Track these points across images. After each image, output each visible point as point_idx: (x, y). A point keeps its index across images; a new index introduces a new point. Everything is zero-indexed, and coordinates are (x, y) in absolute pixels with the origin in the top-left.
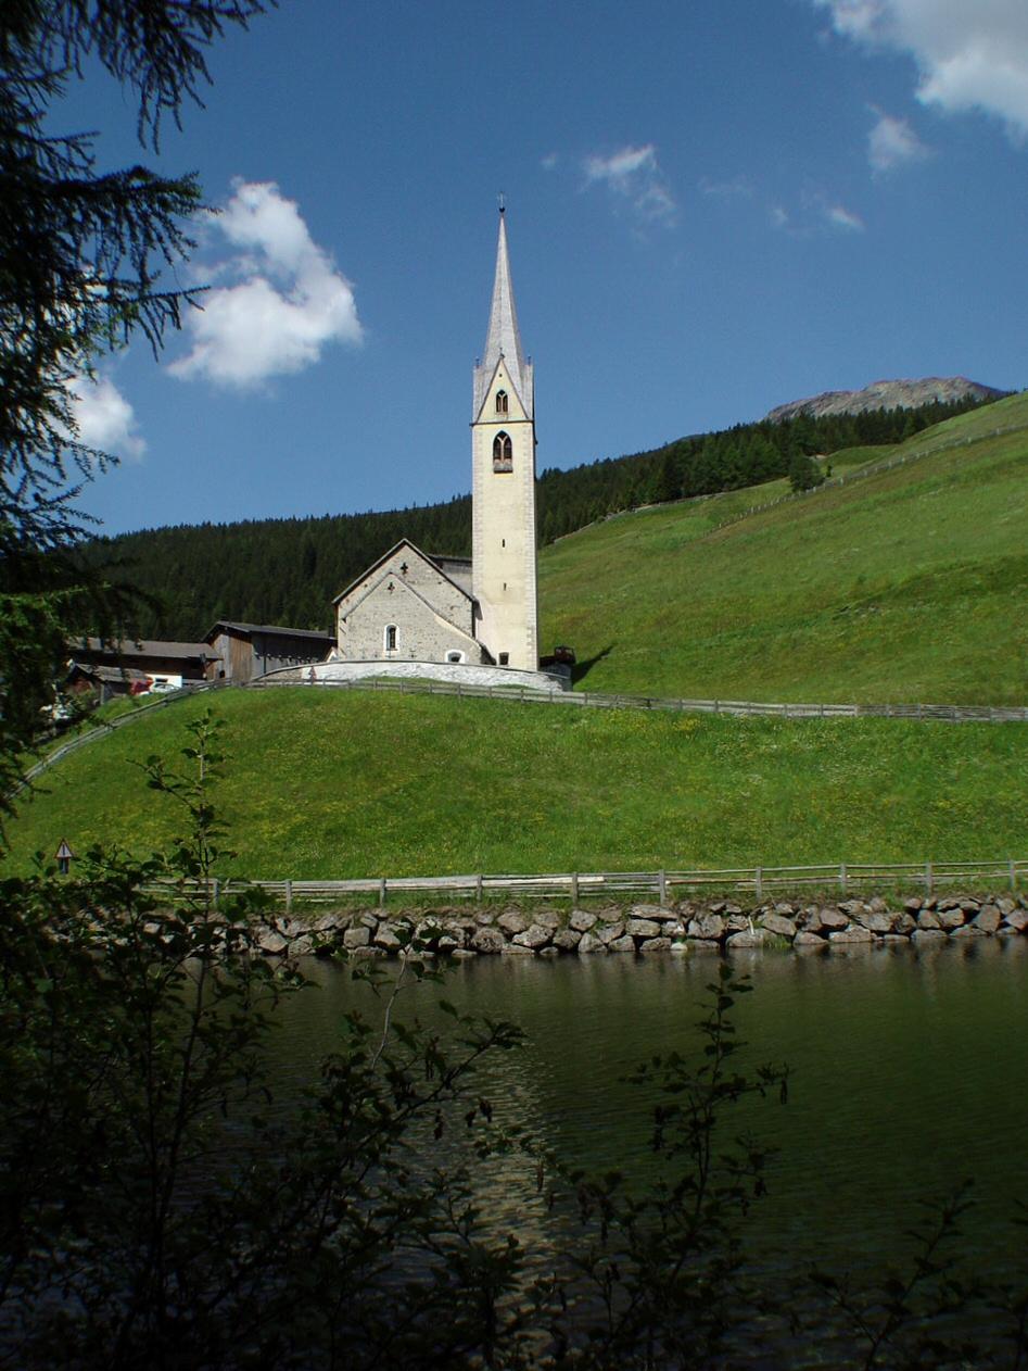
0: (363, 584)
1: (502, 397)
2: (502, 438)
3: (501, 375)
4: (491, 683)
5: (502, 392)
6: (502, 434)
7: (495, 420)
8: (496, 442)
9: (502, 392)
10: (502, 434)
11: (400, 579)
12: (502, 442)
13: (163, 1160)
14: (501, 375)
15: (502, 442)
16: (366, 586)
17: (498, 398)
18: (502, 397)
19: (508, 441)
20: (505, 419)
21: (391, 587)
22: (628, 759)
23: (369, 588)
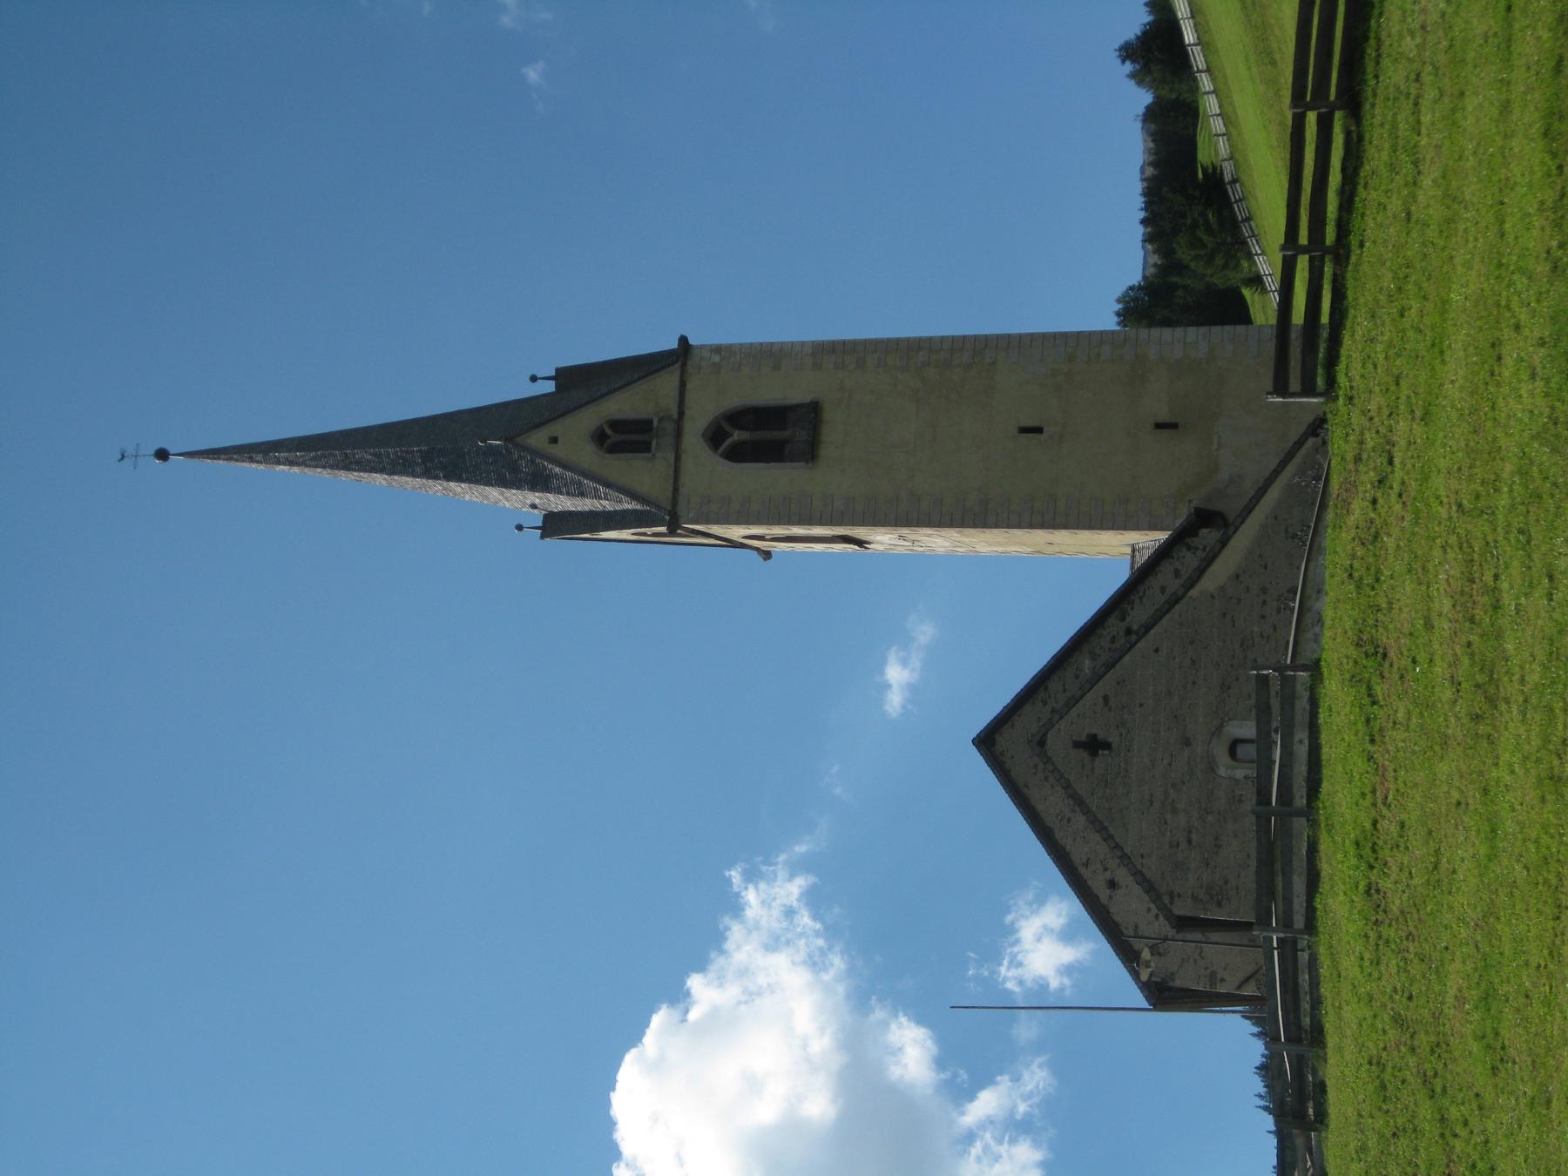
0: (1103, 893)
1: (615, 437)
2: (727, 435)
3: (554, 440)
4: (1296, 771)
5: (600, 438)
6: (715, 437)
7: (671, 456)
8: (737, 454)
9: (600, 438)
10: (715, 437)
11: (678, 434)
12: (737, 435)
13: (1558, 942)
14: (554, 440)
15: (737, 435)
16: (1112, 884)
17: (612, 450)
18: (615, 437)
19: (737, 418)
20: (670, 427)
21: (1094, 746)
22: (1498, 384)
23: (1122, 875)
